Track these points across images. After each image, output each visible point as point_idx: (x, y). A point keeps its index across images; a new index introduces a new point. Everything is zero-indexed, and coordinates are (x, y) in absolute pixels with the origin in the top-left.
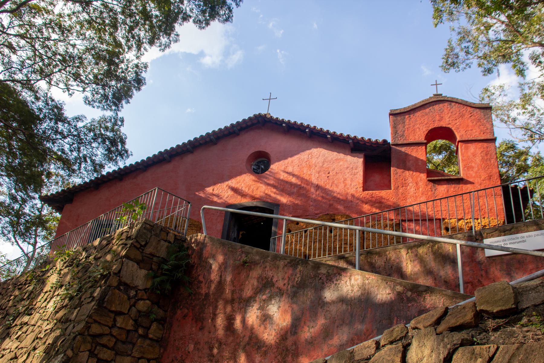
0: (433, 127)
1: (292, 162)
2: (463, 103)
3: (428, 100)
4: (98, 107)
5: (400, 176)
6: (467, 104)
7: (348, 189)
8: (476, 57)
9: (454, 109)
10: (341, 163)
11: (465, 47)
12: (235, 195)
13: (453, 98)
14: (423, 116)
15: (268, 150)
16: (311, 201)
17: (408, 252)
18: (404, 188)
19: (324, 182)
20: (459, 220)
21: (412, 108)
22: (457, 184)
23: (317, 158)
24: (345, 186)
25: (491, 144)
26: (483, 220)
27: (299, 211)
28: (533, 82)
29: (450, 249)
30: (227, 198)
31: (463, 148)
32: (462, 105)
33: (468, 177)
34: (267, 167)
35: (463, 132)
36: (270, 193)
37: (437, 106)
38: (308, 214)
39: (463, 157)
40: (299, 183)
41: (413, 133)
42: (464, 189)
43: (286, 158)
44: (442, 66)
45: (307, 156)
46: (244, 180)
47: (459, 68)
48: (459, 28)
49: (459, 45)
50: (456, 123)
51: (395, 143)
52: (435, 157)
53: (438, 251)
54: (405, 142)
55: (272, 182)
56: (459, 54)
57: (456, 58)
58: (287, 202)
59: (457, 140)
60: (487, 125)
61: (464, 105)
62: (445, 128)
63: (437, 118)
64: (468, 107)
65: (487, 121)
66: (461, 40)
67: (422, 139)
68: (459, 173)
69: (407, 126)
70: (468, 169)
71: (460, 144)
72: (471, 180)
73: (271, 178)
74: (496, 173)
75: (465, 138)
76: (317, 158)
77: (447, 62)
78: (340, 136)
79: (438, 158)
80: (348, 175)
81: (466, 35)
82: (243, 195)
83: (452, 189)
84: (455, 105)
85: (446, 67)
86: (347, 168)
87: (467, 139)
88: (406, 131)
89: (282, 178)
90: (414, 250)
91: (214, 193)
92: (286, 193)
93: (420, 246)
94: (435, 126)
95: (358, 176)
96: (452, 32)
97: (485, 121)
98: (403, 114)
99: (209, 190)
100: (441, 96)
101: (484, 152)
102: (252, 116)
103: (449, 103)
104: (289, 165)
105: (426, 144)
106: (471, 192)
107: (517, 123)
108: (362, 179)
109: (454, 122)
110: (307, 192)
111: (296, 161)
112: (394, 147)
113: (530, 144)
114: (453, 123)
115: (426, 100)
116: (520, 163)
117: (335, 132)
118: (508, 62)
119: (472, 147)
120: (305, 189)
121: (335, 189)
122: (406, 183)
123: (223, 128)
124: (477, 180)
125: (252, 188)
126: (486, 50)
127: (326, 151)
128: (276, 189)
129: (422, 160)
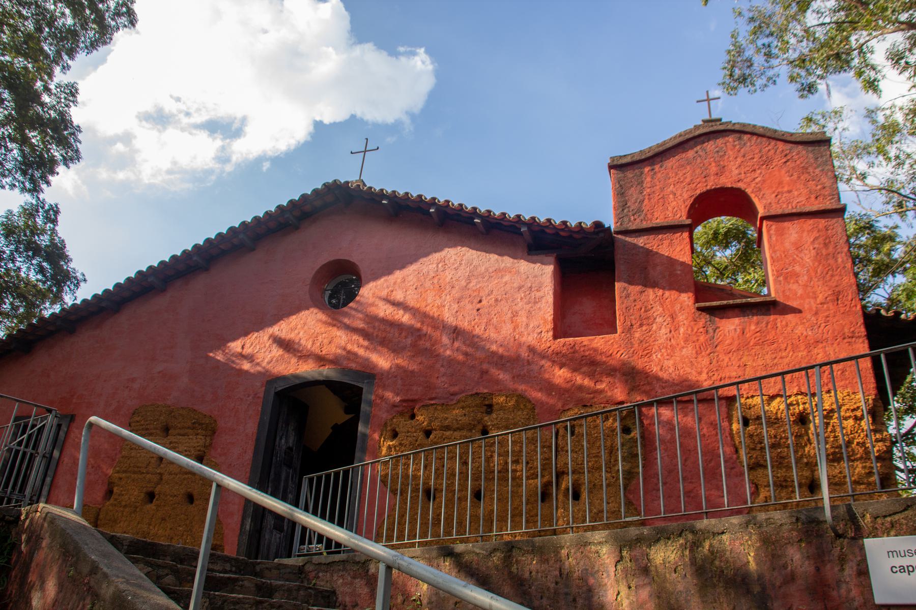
0: (705, 190)
1: (404, 280)
2: (768, 134)
3: (690, 131)
4: (13, 186)
5: (635, 301)
6: (776, 136)
7: (521, 334)
8: (785, 62)
9: (747, 148)
10: (507, 278)
11: (764, 45)
12: (286, 356)
13: (744, 125)
14: (683, 166)
15: (354, 258)
16: (442, 366)
17: (621, 558)
18: (644, 328)
19: (470, 322)
20: (772, 398)
21: (657, 150)
22: (763, 314)
23: (456, 269)
24: (514, 329)
25: (834, 220)
26: (825, 396)
27: (415, 388)
28: (894, 106)
29: (751, 559)
30: (269, 363)
31: (772, 232)
32: (764, 139)
33: (788, 298)
34: (352, 296)
35: (770, 198)
36: (355, 349)
37: (711, 143)
38: (434, 396)
39: (774, 252)
40: (418, 325)
41: (661, 204)
42: (779, 325)
43: (389, 271)
44: (723, 83)
45: (435, 266)
46: (305, 324)
47: (754, 85)
48: (750, 10)
49: (753, 42)
50: (754, 179)
51: (622, 228)
52: (718, 254)
53: (712, 562)
54: (645, 225)
55: (361, 325)
56: (753, 58)
57: (749, 67)
58: (391, 368)
59: (759, 216)
60: (824, 179)
61: (769, 138)
62: (732, 189)
63: (713, 169)
64: (778, 143)
65: (823, 170)
66: (755, 33)
67: (682, 217)
68: (765, 283)
69: (648, 190)
70: (786, 278)
71: (764, 222)
72: (794, 304)
73: (360, 315)
74: (851, 286)
75: (776, 210)
76: (456, 269)
77: (731, 75)
78: (502, 219)
79: (724, 255)
80: (520, 304)
81: (764, 23)
82: (303, 356)
83: (753, 327)
84: (749, 140)
85: (731, 84)
86: (520, 288)
87: (779, 212)
88: (646, 202)
89: (381, 314)
90: (637, 552)
91: (244, 353)
92: (389, 349)
93: (658, 540)
94: (708, 188)
95: (542, 304)
96: (738, 19)
97: (817, 171)
98: (639, 165)
99: (235, 346)
100: (718, 123)
101: (821, 240)
102: (320, 187)
103: (737, 135)
104: (397, 287)
105: (690, 228)
106: (813, 367)
107: (871, 181)
108: (552, 312)
109: (750, 176)
110: (433, 345)
111: (411, 278)
112: (619, 236)
113: (896, 219)
114: (748, 180)
115: (686, 133)
116: (878, 258)
117: (489, 211)
118: (845, 70)
119: (793, 230)
120: (430, 337)
121: (494, 336)
122: (648, 318)
123: (261, 216)
124: (808, 305)
125: (320, 340)
126: (805, 47)
127: (474, 252)
128: (369, 340)
129: (683, 263)
